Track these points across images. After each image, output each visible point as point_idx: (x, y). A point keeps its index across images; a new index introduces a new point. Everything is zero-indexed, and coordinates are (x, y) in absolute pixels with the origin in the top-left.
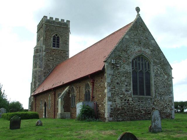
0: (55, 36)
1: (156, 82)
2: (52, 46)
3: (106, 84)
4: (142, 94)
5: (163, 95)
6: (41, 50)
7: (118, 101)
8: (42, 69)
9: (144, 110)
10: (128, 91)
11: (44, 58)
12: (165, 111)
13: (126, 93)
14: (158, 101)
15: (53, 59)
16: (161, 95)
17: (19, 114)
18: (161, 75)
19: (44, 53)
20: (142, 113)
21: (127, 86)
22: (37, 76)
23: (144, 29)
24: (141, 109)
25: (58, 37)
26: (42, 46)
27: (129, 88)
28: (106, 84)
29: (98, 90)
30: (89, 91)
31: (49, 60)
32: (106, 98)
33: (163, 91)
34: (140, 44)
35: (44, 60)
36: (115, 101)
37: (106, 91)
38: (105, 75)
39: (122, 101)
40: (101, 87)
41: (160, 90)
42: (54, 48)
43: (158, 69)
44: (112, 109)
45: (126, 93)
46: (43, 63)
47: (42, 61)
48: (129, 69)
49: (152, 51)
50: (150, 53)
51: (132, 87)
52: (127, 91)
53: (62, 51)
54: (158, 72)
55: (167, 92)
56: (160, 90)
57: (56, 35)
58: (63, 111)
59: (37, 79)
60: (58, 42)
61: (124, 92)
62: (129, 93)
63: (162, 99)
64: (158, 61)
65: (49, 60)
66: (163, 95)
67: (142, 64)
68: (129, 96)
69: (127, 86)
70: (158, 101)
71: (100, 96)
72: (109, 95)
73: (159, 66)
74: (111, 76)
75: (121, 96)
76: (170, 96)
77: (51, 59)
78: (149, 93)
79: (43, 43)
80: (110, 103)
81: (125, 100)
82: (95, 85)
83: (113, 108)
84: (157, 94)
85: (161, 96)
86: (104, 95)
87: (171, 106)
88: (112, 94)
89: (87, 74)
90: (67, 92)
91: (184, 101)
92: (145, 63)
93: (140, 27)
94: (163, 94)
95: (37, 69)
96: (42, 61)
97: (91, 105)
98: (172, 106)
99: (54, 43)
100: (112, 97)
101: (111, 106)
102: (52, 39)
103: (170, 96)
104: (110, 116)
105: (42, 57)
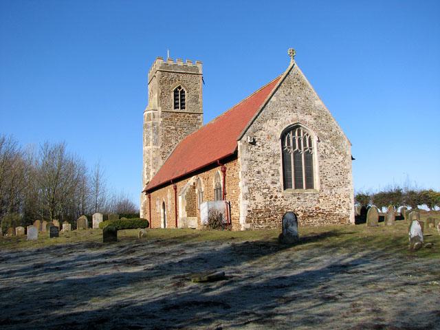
0: (176, 89)
3: (240, 173)
4: (298, 186)
6: (156, 115)
7: (259, 198)
8: (159, 147)
9: (302, 211)
10: (276, 183)
11: (161, 128)
12: (337, 212)
13: (272, 187)
14: (326, 196)
15: (176, 130)
16: (331, 187)
17: (385, 194)
18: (332, 156)
19: (162, 119)
21: (273, 175)
22: (151, 158)
23: (303, 84)
24: (296, 210)
25: (183, 92)
26: (157, 108)
27: (277, 178)
28: (240, 173)
29: (230, 182)
30: (219, 184)
31: (168, 132)
32: (241, 196)
35: (160, 132)
36: (254, 200)
37: (240, 184)
38: (239, 160)
39: (265, 198)
40: (235, 179)
41: (329, 179)
42: (176, 110)
43: (325, 146)
44: (249, 211)
45: (272, 187)
46: (161, 136)
47: (157, 133)
48: (276, 149)
49: (315, 119)
50: (312, 121)
53: (190, 113)
54: (327, 151)
55: (341, 182)
56: (329, 179)
57: (180, 88)
58: (186, 215)
59: (151, 164)
60: (183, 100)
61: (269, 184)
62: (277, 186)
63: (334, 193)
64: (326, 134)
65: (168, 132)
67: (294, 140)
68: (277, 191)
69: (273, 175)
70: (326, 196)
71: (234, 192)
72: (245, 190)
73: (328, 141)
74: (247, 162)
75: (265, 191)
76: (347, 189)
78: (310, 185)
79: (158, 103)
80: (247, 202)
82: (227, 175)
83: (251, 209)
84: (324, 186)
86: (238, 191)
87: (348, 204)
88: (249, 189)
89: (215, 159)
90: (191, 186)
91: (427, 190)
93: (295, 80)
95: (150, 147)
96: (157, 133)
97: (221, 206)
98: (350, 204)
99: (183, 98)
100: (250, 193)
101: (249, 206)
102: (172, 94)
103: (347, 189)
104: (247, 222)
105: (158, 128)
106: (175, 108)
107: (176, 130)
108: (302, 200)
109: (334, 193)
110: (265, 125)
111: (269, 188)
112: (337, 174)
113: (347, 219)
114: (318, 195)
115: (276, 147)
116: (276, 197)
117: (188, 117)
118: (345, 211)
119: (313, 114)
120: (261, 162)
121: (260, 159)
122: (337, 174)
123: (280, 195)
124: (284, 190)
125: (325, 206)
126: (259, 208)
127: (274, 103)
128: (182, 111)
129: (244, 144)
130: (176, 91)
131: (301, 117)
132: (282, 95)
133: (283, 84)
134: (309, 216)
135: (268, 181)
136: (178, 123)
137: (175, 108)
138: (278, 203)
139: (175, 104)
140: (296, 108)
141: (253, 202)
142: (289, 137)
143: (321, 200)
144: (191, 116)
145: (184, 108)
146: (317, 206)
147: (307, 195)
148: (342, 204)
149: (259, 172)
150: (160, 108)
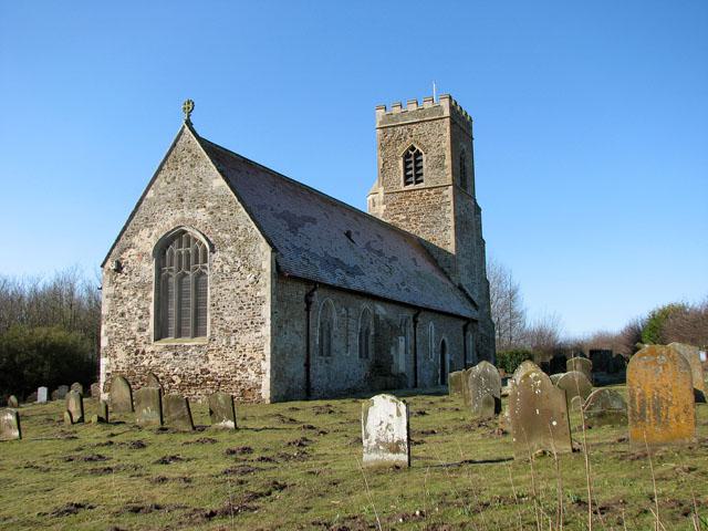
1: (216, 299)
2: (402, 183)
5: (236, 331)
9: (180, 376)
13: (138, 335)
15: (407, 220)
18: (235, 274)
20: (174, 382)
21: (141, 317)
33: (236, 321)
34: (182, 200)
36: (115, 357)
41: (227, 319)
42: (408, 188)
45: (138, 335)
49: (212, 213)
51: (152, 321)
52: (141, 330)
53: (430, 189)
54: (226, 268)
55: (249, 323)
63: (233, 342)
64: (227, 236)
66: (236, 331)
69: (141, 317)
76: (260, 334)
77: (403, 220)
81: (137, 353)
85: (229, 337)
92: (197, 251)
94: (234, 328)
98: (262, 363)
102: (401, 163)
103: (260, 334)
106: (407, 184)
107: (407, 220)
108: (181, 356)
109: (233, 342)
110: (135, 240)
111: (134, 339)
112: (241, 308)
113: (257, 392)
114: (206, 348)
115: (148, 270)
116: (143, 353)
117: (428, 195)
118: (253, 377)
119: (208, 204)
120: (127, 299)
121: (125, 293)
122: (241, 308)
123: (149, 349)
124: (155, 340)
125: (216, 365)
126: (121, 369)
127: (150, 200)
128: (417, 186)
129: (107, 273)
130: (407, 156)
131: (188, 215)
132: (163, 184)
133: (165, 167)
134: (190, 384)
135: (134, 328)
136: (412, 209)
137: (407, 184)
138: (146, 362)
139: (406, 177)
140: (182, 200)
141: (113, 361)
142: (172, 253)
143: (210, 356)
144: (432, 192)
145: (422, 181)
146: (205, 366)
147: (189, 347)
148: (247, 364)
149: (123, 315)
150: (382, 189)
